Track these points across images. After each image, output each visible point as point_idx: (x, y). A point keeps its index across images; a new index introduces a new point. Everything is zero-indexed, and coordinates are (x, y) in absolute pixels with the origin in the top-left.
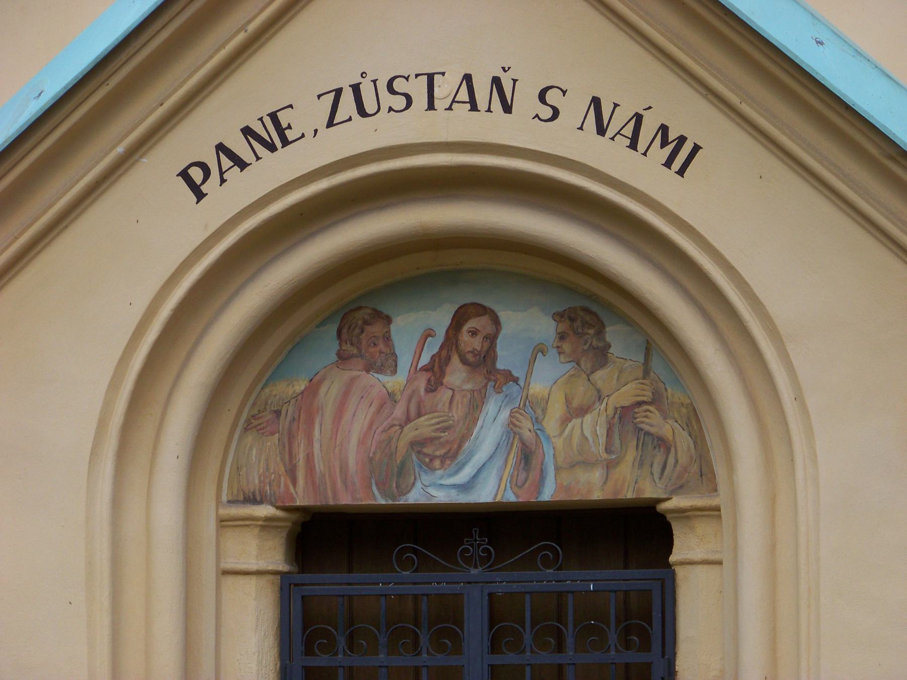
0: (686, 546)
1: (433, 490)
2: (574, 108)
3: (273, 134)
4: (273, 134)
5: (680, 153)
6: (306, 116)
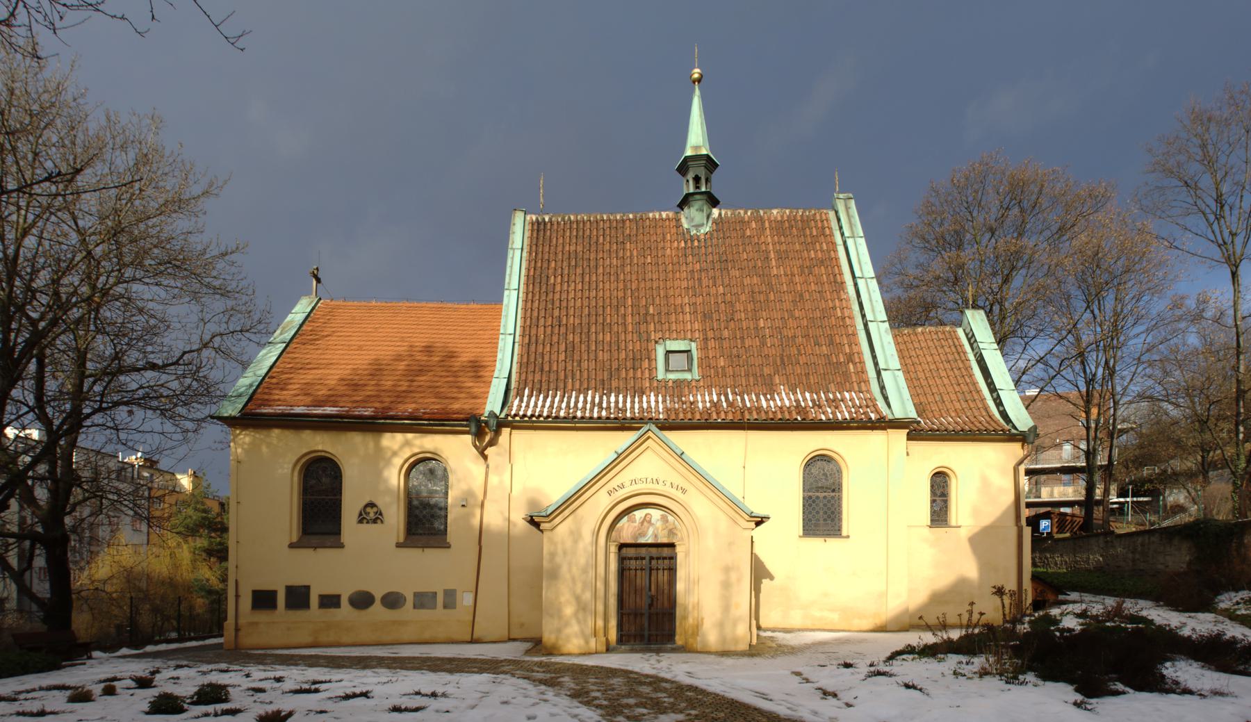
0: (678, 549)
1: (642, 541)
2: (668, 484)
3: (622, 486)
4: (622, 486)
5: (684, 491)
6: (627, 484)
